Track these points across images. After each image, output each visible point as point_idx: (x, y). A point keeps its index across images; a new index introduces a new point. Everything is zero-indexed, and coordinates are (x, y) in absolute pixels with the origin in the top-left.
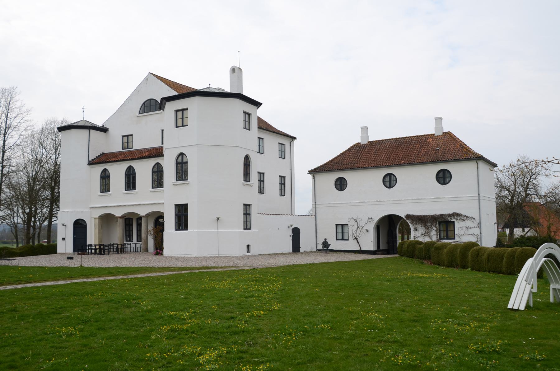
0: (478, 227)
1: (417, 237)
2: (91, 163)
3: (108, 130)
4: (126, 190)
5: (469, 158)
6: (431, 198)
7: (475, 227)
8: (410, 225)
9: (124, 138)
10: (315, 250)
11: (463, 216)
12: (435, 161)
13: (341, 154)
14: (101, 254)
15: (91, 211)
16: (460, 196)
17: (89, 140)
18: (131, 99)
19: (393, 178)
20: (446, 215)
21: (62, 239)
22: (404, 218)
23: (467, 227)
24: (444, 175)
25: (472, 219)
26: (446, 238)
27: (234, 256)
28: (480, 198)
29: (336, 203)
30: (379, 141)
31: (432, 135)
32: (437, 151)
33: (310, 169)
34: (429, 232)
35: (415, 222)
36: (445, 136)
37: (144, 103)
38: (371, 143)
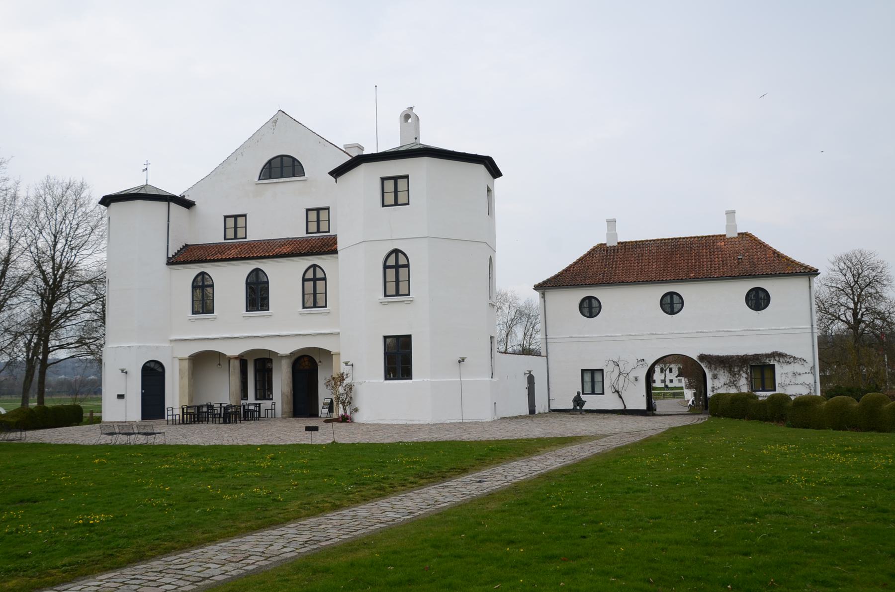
0: (812, 373)
1: (717, 388)
2: (173, 261)
3: (195, 205)
4: (247, 311)
5: (680, 278)
6: (739, 329)
7: (806, 373)
8: (706, 370)
9: (228, 219)
10: (547, 411)
11: (788, 357)
12: (745, 275)
13: (579, 260)
14: (225, 422)
15: (172, 346)
16: (784, 328)
17: (168, 221)
18: (242, 153)
19: (595, 303)
20: (762, 354)
21: (116, 397)
22: (696, 360)
23: (794, 373)
24: (757, 296)
25: (802, 361)
26: (761, 389)
27: (484, 421)
28: (548, 342)
29: (582, 336)
30: (636, 242)
31: (721, 236)
32: (740, 260)
33: (537, 283)
34: (736, 381)
35: (713, 366)
36: (744, 239)
37: (270, 162)
38: (625, 246)
